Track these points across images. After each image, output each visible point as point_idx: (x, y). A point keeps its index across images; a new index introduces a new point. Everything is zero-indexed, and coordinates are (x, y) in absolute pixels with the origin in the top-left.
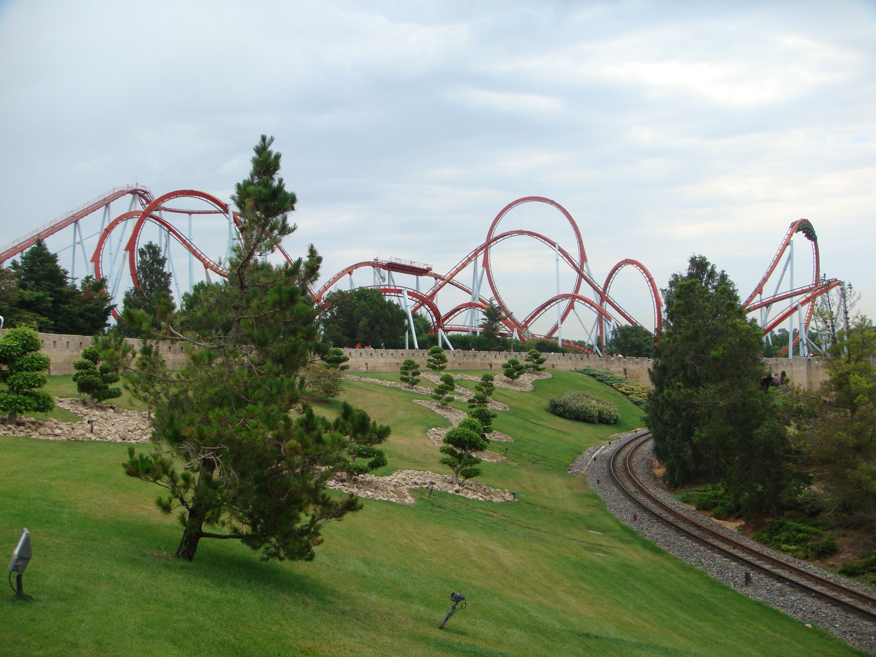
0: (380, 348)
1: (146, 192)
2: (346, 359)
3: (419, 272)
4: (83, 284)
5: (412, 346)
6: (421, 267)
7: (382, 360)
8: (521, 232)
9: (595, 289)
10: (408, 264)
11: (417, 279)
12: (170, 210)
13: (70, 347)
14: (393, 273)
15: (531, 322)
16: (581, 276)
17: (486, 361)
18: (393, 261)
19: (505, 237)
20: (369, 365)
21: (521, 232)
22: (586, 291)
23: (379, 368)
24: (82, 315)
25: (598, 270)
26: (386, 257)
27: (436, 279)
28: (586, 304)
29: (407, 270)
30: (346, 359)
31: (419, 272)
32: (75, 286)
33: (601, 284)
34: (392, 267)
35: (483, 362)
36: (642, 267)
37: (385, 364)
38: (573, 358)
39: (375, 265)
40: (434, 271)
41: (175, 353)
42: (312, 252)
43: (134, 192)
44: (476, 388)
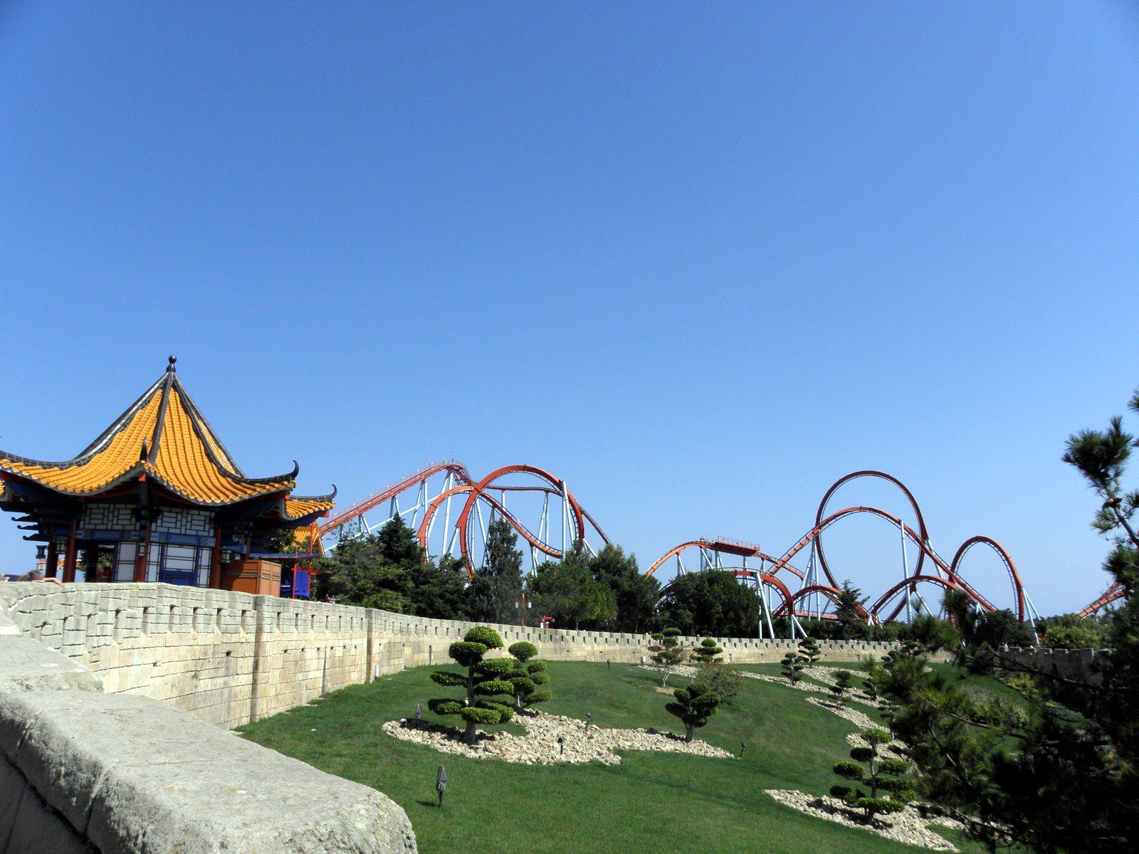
0: (283, 582)
1: (460, 468)
2: (719, 651)
3: (746, 552)
4: (441, 563)
5: (767, 635)
6: (749, 547)
7: (746, 651)
8: (862, 509)
9: (944, 569)
10: (735, 544)
11: (744, 560)
12: (494, 488)
13: (449, 634)
14: (720, 553)
15: (881, 607)
16: (924, 551)
17: (854, 652)
18: (721, 541)
19: (837, 518)
20: (733, 656)
21: (862, 509)
22: (929, 568)
23: (743, 660)
24: (441, 596)
25: (943, 547)
26: (713, 539)
27: (763, 559)
28: (937, 583)
29: (738, 551)
30: (719, 651)
31: (746, 552)
32: (433, 564)
33: (949, 562)
34: (719, 547)
35: (850, 653)
36: (992, 542)
37: (749, 655)
38: (866, 646)
39: (701, 544)
40: (762, 551)
41: (544, 642)
42: (521, 552)
43: (450, 468)
44: (864, 684)
